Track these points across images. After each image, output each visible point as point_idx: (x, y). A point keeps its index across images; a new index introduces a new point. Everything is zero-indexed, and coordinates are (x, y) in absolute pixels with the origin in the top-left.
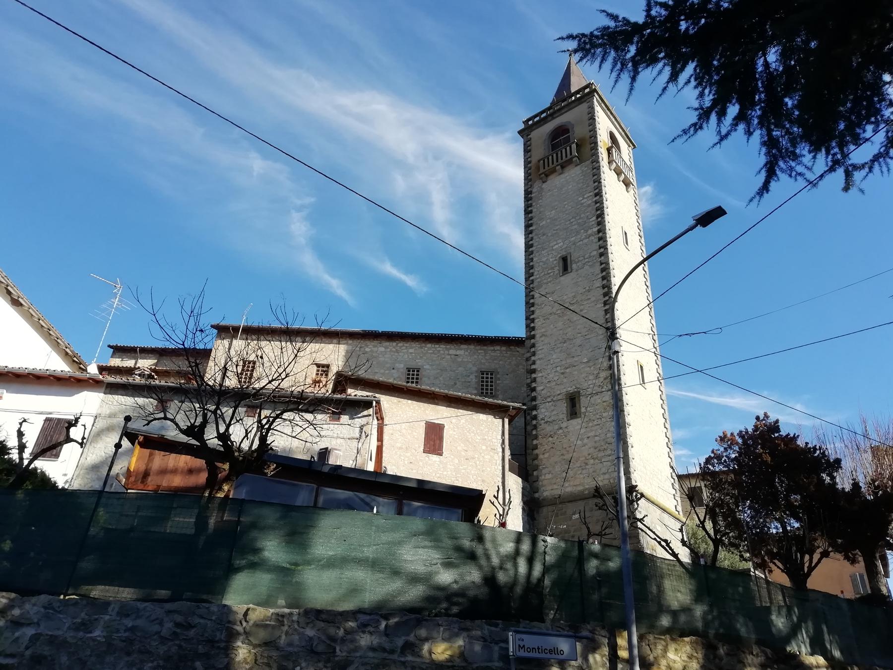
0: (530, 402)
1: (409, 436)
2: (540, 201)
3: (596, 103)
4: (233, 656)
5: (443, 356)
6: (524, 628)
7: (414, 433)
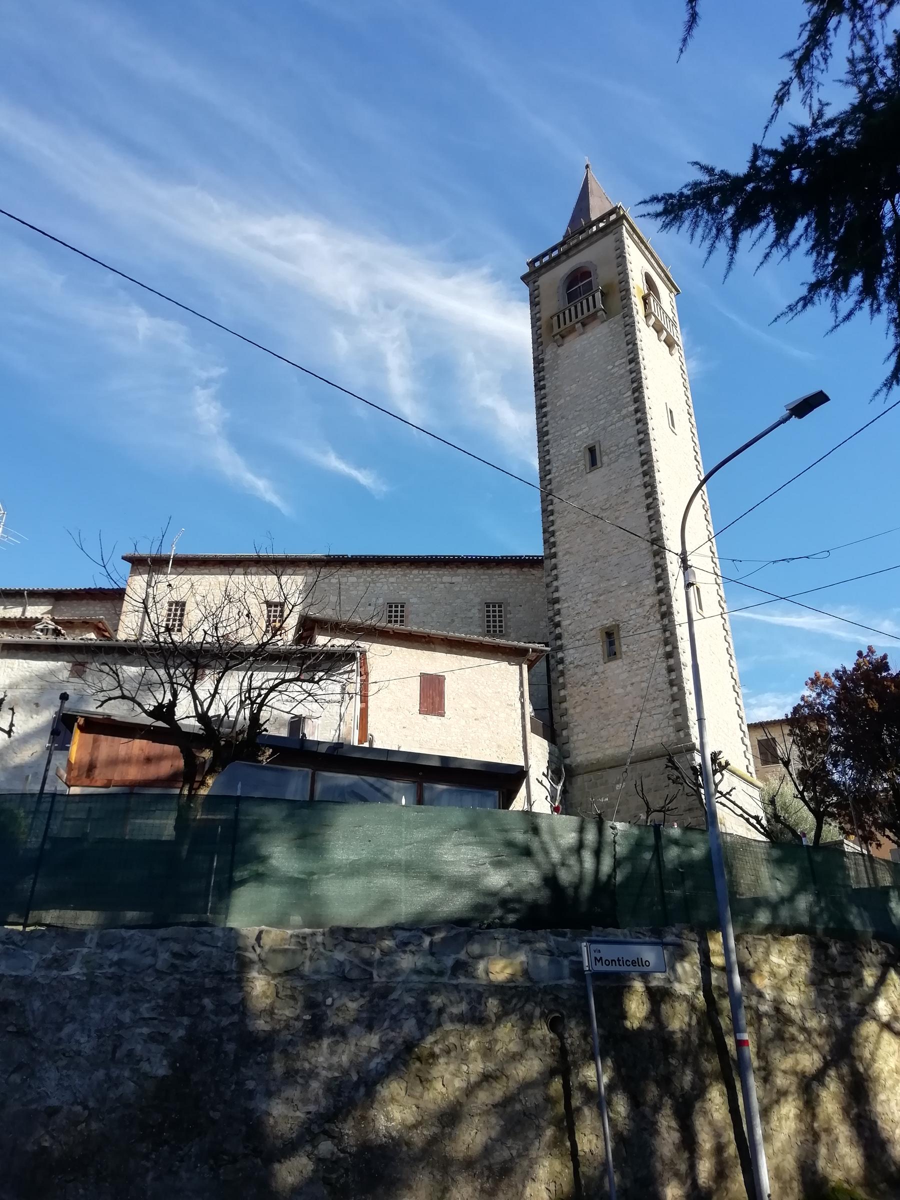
2: (556, 372)
3: (625, 234)
4: (249, 989)
5: (435, 585)
6: (598, 936)
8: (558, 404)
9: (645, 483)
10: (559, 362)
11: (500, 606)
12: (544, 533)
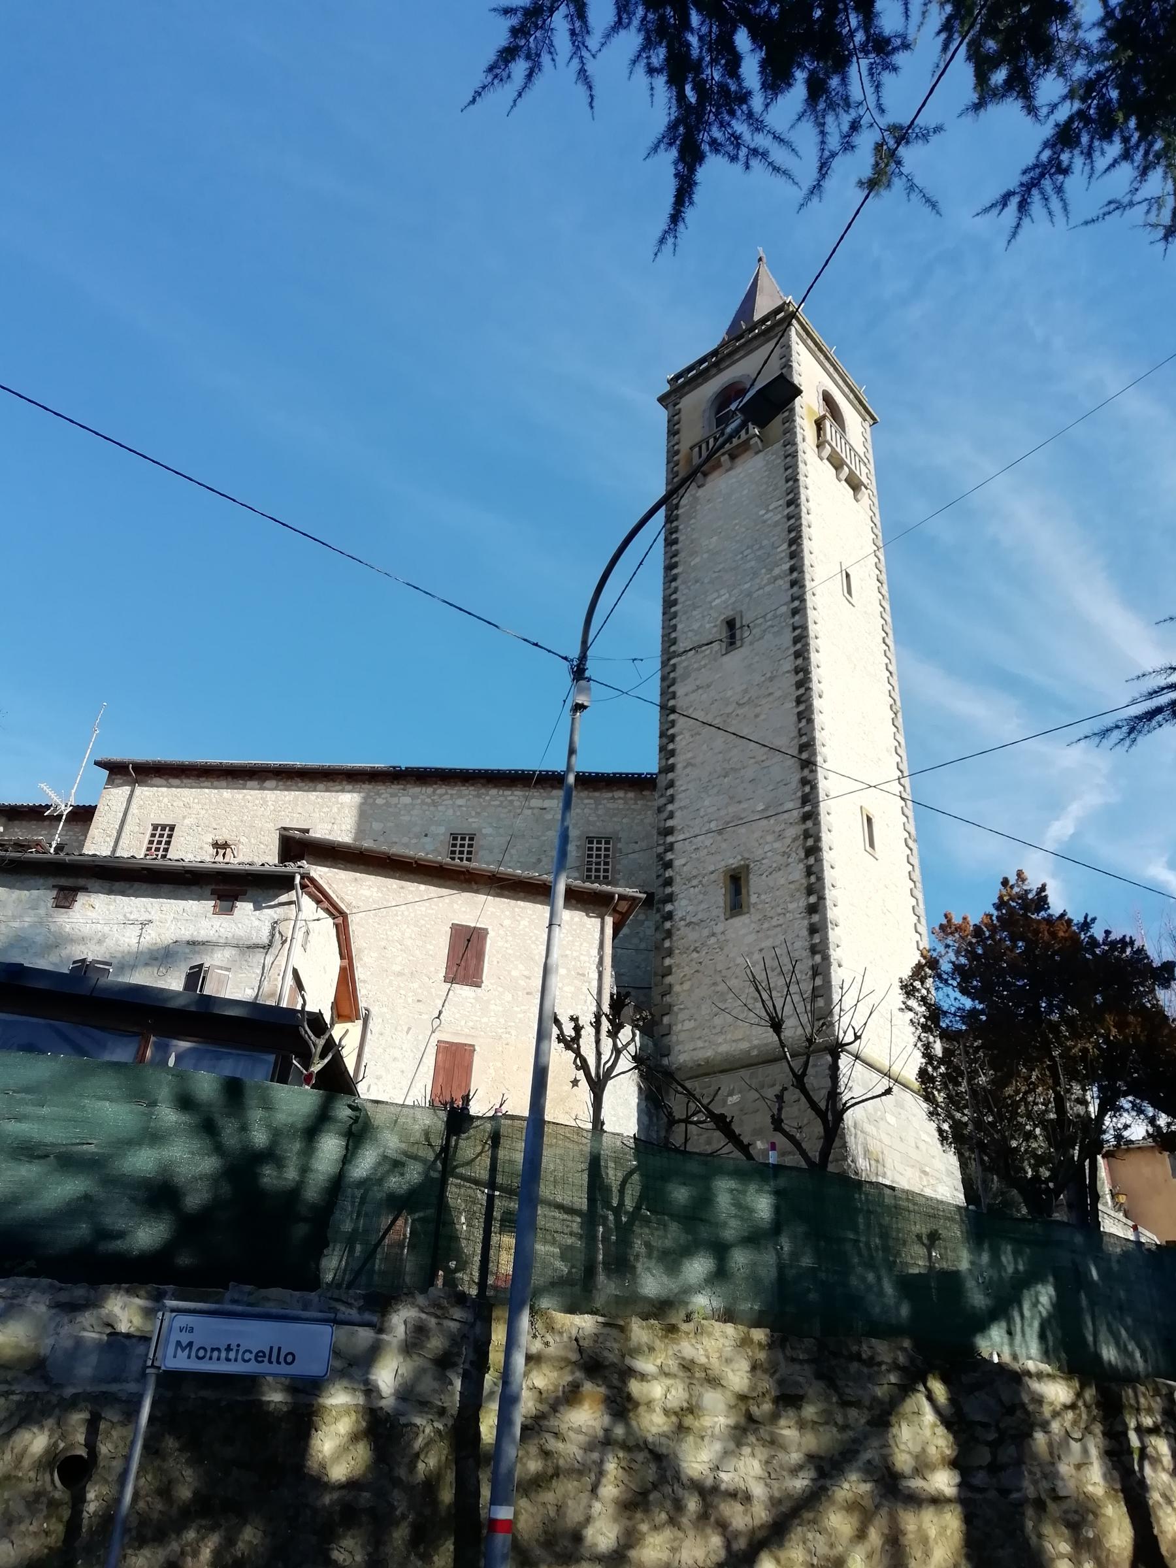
0: (661, 889)
1: (417, 952)
2: (693, 521)
6: (234, 1301)
7: (429, 946)
8: (692, 564)
9: (796, 667)
10: (698, 507)
11: (607, 843)
12: (661, 737)
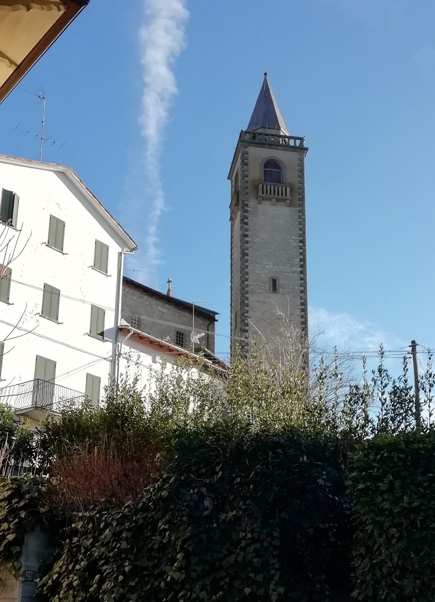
10: (258, 213)
